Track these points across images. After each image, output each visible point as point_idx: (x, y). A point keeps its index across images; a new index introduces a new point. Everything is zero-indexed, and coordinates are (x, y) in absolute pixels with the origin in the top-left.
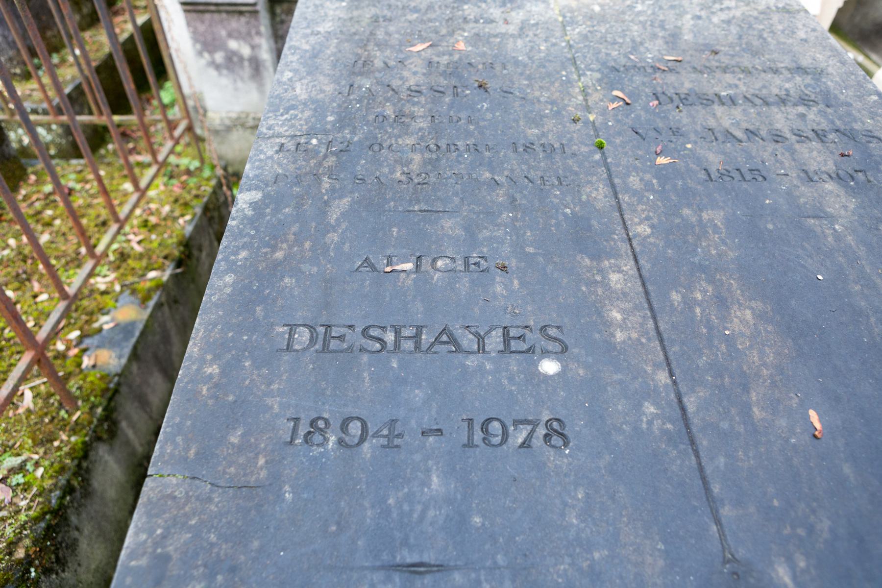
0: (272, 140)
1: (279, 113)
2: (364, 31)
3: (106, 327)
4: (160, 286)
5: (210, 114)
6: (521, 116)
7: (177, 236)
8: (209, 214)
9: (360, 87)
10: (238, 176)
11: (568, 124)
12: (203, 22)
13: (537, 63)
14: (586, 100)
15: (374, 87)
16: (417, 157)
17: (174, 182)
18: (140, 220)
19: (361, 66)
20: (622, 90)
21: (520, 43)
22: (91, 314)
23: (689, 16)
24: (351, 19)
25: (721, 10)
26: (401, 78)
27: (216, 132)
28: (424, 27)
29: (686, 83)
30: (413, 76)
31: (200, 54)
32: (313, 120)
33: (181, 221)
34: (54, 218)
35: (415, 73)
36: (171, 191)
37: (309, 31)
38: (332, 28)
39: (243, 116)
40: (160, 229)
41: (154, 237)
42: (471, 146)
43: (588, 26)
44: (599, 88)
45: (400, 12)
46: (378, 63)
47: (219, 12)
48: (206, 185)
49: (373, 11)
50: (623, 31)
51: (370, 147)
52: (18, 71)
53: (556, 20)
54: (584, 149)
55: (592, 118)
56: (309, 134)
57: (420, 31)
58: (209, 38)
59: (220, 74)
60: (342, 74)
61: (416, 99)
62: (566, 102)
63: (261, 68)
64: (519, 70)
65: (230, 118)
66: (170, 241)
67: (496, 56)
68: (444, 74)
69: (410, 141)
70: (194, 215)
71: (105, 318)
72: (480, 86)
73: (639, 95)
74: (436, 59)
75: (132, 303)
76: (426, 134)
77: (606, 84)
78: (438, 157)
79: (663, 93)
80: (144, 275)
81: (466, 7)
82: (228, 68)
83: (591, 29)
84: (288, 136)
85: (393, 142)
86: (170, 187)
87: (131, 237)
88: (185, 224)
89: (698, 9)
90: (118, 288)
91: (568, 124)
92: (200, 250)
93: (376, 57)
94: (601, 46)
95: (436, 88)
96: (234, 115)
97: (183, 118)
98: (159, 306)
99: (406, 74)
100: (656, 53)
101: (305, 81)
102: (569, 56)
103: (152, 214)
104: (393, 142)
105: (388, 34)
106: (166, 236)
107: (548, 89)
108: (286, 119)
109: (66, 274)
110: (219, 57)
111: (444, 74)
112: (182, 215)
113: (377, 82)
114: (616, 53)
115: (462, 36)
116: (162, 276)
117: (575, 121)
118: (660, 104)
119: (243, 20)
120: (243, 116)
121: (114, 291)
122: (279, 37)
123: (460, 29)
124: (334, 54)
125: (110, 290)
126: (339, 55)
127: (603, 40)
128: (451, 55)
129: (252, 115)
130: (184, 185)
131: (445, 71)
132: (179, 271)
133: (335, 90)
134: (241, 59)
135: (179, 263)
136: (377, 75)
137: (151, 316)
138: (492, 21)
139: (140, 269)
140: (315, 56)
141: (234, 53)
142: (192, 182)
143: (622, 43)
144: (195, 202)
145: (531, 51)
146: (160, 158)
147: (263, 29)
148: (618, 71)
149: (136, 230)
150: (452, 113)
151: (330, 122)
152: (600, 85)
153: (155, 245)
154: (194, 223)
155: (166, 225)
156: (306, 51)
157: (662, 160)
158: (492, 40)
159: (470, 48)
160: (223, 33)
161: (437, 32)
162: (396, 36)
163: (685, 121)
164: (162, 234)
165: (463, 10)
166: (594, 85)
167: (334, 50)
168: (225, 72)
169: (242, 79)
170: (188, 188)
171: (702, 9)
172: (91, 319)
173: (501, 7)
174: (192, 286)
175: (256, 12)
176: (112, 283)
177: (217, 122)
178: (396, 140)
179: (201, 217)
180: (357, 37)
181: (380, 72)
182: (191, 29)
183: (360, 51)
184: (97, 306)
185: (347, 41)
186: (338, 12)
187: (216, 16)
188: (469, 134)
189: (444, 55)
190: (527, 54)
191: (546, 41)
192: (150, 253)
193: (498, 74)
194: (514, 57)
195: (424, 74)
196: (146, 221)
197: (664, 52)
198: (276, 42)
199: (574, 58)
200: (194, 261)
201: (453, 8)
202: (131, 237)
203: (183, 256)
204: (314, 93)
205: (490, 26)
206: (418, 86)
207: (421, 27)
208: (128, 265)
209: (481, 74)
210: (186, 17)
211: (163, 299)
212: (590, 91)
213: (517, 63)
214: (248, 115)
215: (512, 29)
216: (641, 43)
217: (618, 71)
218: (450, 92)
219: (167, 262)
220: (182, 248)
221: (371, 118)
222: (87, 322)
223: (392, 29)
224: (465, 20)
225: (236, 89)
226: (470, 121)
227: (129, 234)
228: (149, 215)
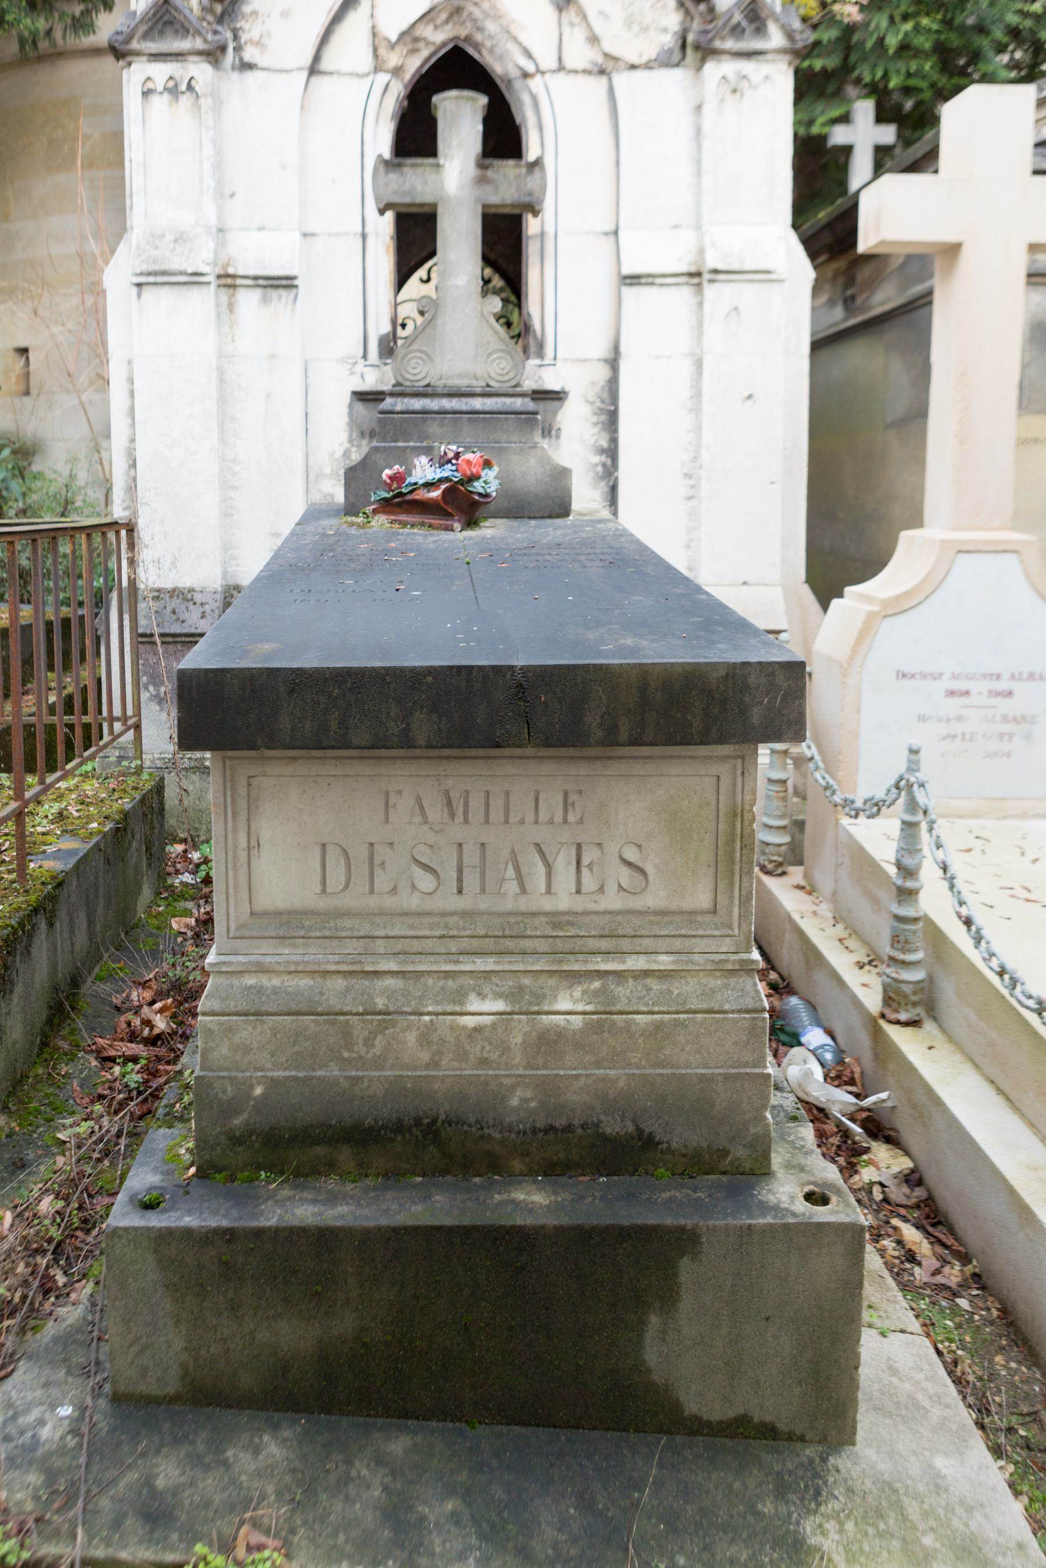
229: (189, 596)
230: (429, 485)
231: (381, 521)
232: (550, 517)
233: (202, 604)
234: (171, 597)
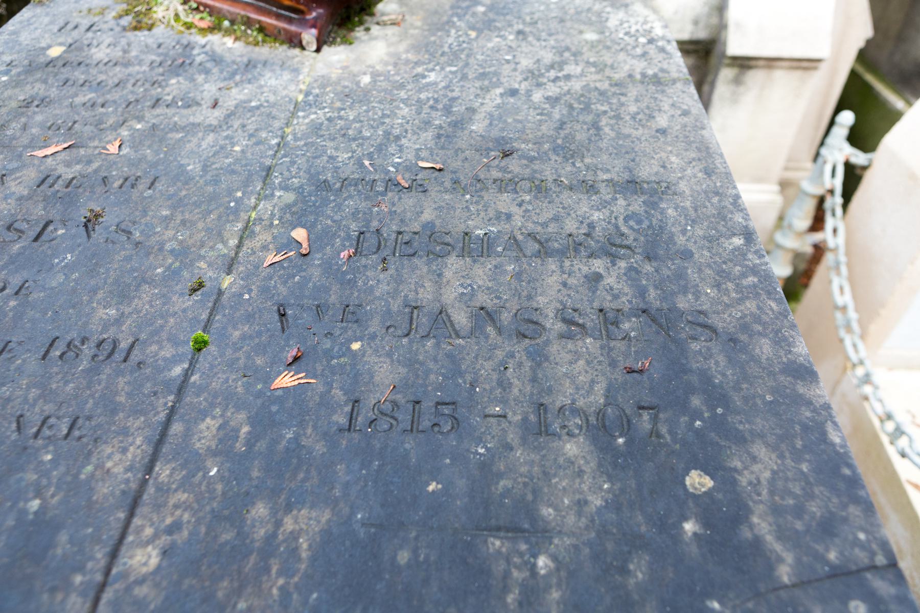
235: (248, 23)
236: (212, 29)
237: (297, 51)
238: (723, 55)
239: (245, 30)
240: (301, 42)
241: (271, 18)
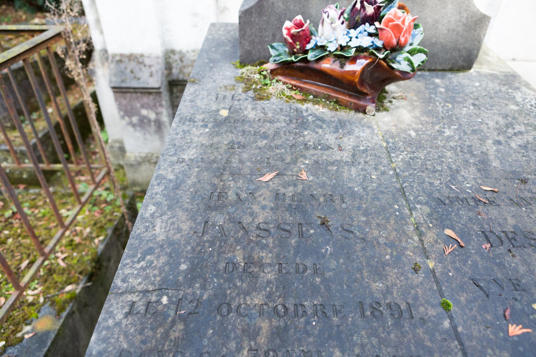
0: (124, 297)
1: (136, 259)
2: (222, 159)
3: (26, 336)
4: (74, 298)
5: (128, 154)
6: (364, 264)
7: (92, 253)
8: (117, 233)
9: (214, 225)
10: (144, 192)
11: (410, 275)
12: (125, 98)
13: (371, 193)
14: (421, 241)
15: (226, 225)
16: (265, 325)
17: (96, 208)
18: (68, 239)
19: (214, 200)
20: (452, 228)
21: (353, 170)
22: (17, 324)
23: (490, 141)
24: (212, 145)
25: (515, 134)
26: (251, 214)
27: (132, 165)
28: (272, 154)
29: (508, 218)
30: (261, 213)
31: (123, 117)
32: (167, 268)
33: (96, 241)
34: (7, 238)
35: (264, 208)
36: (93, 216)
37: (175, 159)
38: (195, 156)
39: (150, 155)
40: (81, 247)
41: (75, 254)
42: (319, 308)
43: (409, 153)
44: (431, 225)
45: (252, 138)
46: (231, 196)
47: (136, 93)
48: (118, 211)
49: (231, 137)
50: (439, 157)
51: (219, 309)
52: (9, 125)
53: (381, 146)
54: (432, 312)
55: (431, 264)
56: (160, 290)
57: (268, 158)
58: (129, 108)
59: (135, 130)
60: (199, 209)
61: (264, 241)
62: (403, 244)
63: (162, 126)
64: (356, 204)
65: (141, 157)
66: (86, 258)
67: (334, 187)
68: (289, 208)
69: (257, 300)
70: (106, 236)
71: (28, 328)
72: (323, 224)
73: (469, 233)
74: (282, 190)
75: (50, 314)
76: (274, 290)
77: (436, 220)
78: (286, 324)
79: (491, 232)
80: (63, 288)
81: (306, 133)
82: (140, 126)
83: (412, 156)
84: (140, 292)
85: (242, 301)
86: (92, 213)
87: (59, 254)
88: (99, 243)
89: (495, 133)
90: (42, 300)
91: (410, 275)
92: (109, 260)
93: (229, 188)
94: (424, 175)
95: (282, 226)
96: (143, 155)
97: (104, 167)
98: (71, 314)
99: (256, 208)
100: (473, 182)
101: (165, 217)
102: (398, 186)
103: (77, 235)
104: (242, 301)
105: (241, 162)
106: (84, 253)
107: (385, 228)
108: (142, 268)
109: (6, 287)
110: (135, 119)
111: (289, 208)
112: (98, 236)
113: (230, 219)
114: (439, 182)
115: (304, 164)
116: (76, 289)
117: (416, 270)
118: (492, 246)
119: (151, 97)
120: (150, 155)
121: (39, 302)
122: (174, 106)
123: (302, 156)
124: (194, 185)
125: (36, 302)
126: (198, 185)
127: (424, 168)
128: (295, 185)
129: (155, 155)
130: (102, 211)
131: (290, 205)
132: (89, 284)
133: (191, 228)
134: (149, 121)
135: (91, 277)
136: (231, 210)
137: (62, 326)
138: (329, 148)
139: (61, 283)
140: (177, 187)
141: (145, 117)
142: (108, 209)
143: (441, 171)
144: (108, 225)
145: (364, 180)
146: (98, 179)
147: (164, 103)
148: (445, 204)
149: (63, 248)
150: (298, 260)
151: (183, 271)
152: (432, 223)
153: (75, 261)
154: (105, 243)
155: (85, 244)
156: (171, 181)
157: (515, 330)
158: (330, 168)
159: (311, 178)
160: (138, 105)
161: (283, 160)
162: (248, 164)
163: (522, 269)
164: (81, 252)
165: (304, 136)
166: (426, 222)
167: (195, 180)
168: (138, 128)
169: (149, 133)
170: (105, 213)
171: (499, 134)
172: (16, 329)
173: (335, 132)
174: (101, 289)
175: (160, 93)
176: (38, 295)
177: (133, 159)
178: (245, 299)
179: (111, 237)
180: (215, 165)
181: (232, 206)
182: (118, 103)
183: (216, 181)
184: (23, 317)
185: (207, 169)
186: (201, 139)
187: (134, 95)
188: (315, 290)
189: (289, 185)
190: (361, 184)
191: (376, 169)
192: (70, 268)
193: (338, 207)
194: (350, 188)
195: (272, 209)
196: (72, 241)
197: (480, 181)
198: (173, 109)
199: (403, 188)
200: (104, 270)
201: (296, 134)
202: (59, 254)
203: (94, 270)
204: (172, 232)
205: (326, 152)
206: (265, 223)
207: (269, 154)
208: (53, 279)
209: (323, 209)
210: (115, 96)
211: (75, 308)
212: (423, 229)
213: (353, 195)
214: (152, 155)
215: (346, 156)
216: (458, 171)
217: (445, 204)
218: (295, 231)
219: (81, 277)
220: (94, 264)
221: (222, 265)
222: (13, 331)
223: (245, 156)
224: (306, 147)
225: (145, 139)
226: (316, 272)
227: (58, 252)
228: (74, 236)
229: (141, 60)
230: (342, 55)
231: (278, 87)
232: (451, 70)
233: (150, 66)
234: (130, 60)
235: (328, 98)
236: (304, 101)
237: (361, 115)
238: (63, 217)
239: (325, 102)
240: (365, 110)
241: (346, 97)
